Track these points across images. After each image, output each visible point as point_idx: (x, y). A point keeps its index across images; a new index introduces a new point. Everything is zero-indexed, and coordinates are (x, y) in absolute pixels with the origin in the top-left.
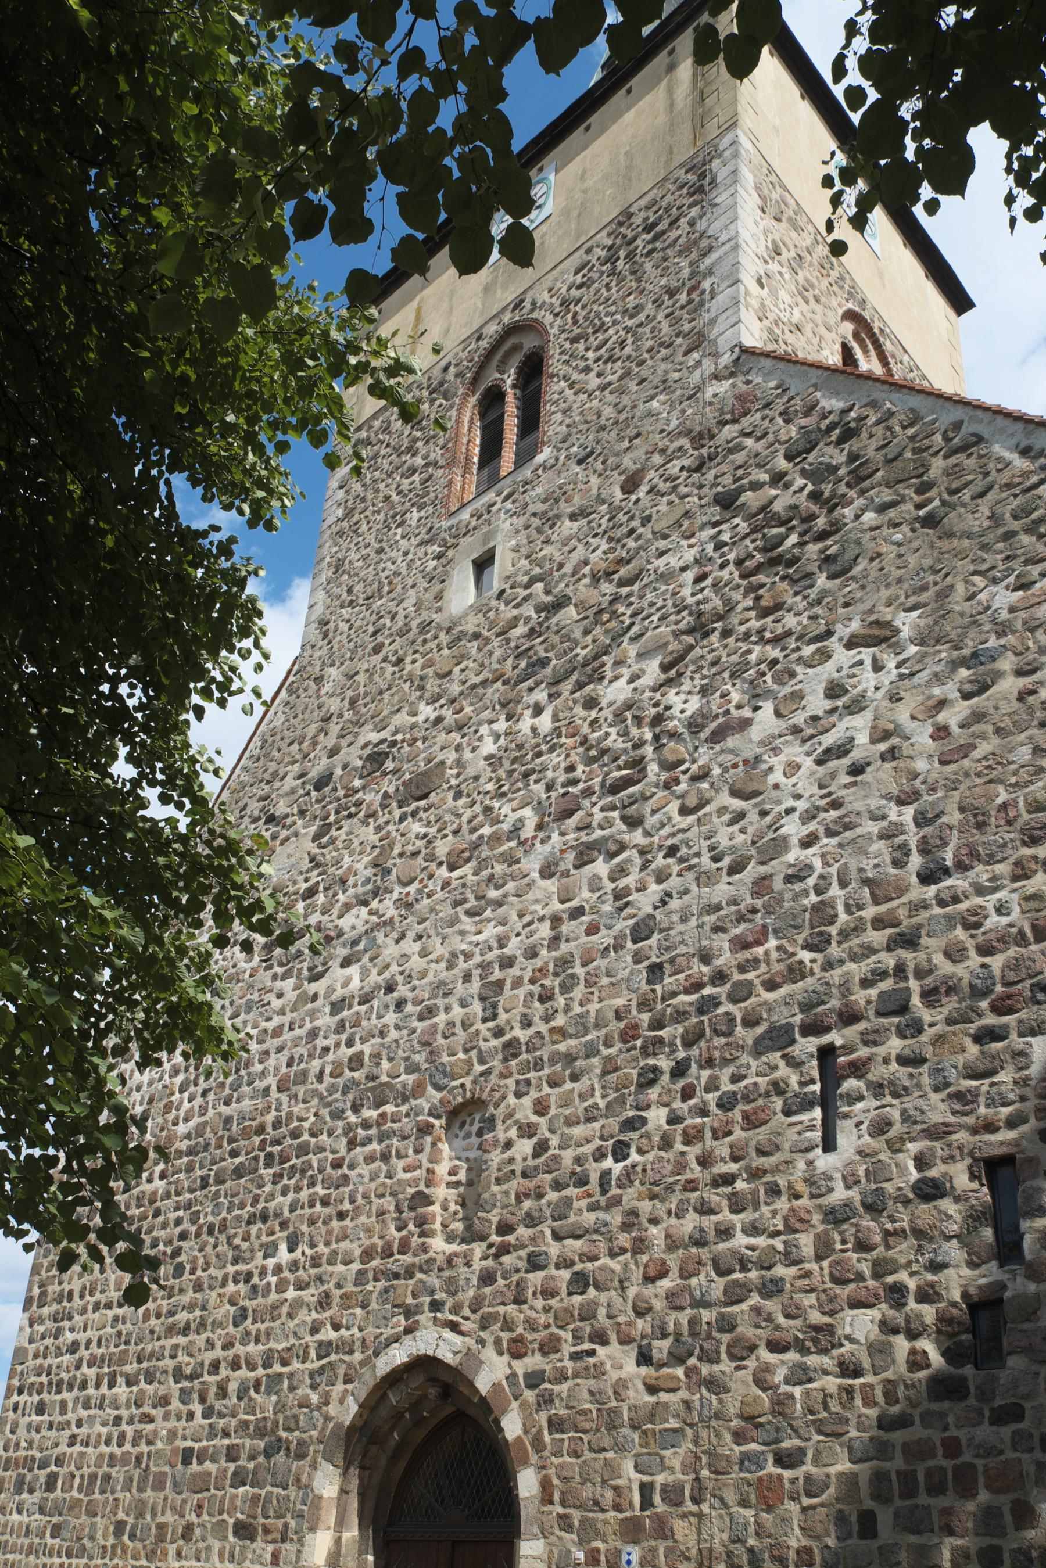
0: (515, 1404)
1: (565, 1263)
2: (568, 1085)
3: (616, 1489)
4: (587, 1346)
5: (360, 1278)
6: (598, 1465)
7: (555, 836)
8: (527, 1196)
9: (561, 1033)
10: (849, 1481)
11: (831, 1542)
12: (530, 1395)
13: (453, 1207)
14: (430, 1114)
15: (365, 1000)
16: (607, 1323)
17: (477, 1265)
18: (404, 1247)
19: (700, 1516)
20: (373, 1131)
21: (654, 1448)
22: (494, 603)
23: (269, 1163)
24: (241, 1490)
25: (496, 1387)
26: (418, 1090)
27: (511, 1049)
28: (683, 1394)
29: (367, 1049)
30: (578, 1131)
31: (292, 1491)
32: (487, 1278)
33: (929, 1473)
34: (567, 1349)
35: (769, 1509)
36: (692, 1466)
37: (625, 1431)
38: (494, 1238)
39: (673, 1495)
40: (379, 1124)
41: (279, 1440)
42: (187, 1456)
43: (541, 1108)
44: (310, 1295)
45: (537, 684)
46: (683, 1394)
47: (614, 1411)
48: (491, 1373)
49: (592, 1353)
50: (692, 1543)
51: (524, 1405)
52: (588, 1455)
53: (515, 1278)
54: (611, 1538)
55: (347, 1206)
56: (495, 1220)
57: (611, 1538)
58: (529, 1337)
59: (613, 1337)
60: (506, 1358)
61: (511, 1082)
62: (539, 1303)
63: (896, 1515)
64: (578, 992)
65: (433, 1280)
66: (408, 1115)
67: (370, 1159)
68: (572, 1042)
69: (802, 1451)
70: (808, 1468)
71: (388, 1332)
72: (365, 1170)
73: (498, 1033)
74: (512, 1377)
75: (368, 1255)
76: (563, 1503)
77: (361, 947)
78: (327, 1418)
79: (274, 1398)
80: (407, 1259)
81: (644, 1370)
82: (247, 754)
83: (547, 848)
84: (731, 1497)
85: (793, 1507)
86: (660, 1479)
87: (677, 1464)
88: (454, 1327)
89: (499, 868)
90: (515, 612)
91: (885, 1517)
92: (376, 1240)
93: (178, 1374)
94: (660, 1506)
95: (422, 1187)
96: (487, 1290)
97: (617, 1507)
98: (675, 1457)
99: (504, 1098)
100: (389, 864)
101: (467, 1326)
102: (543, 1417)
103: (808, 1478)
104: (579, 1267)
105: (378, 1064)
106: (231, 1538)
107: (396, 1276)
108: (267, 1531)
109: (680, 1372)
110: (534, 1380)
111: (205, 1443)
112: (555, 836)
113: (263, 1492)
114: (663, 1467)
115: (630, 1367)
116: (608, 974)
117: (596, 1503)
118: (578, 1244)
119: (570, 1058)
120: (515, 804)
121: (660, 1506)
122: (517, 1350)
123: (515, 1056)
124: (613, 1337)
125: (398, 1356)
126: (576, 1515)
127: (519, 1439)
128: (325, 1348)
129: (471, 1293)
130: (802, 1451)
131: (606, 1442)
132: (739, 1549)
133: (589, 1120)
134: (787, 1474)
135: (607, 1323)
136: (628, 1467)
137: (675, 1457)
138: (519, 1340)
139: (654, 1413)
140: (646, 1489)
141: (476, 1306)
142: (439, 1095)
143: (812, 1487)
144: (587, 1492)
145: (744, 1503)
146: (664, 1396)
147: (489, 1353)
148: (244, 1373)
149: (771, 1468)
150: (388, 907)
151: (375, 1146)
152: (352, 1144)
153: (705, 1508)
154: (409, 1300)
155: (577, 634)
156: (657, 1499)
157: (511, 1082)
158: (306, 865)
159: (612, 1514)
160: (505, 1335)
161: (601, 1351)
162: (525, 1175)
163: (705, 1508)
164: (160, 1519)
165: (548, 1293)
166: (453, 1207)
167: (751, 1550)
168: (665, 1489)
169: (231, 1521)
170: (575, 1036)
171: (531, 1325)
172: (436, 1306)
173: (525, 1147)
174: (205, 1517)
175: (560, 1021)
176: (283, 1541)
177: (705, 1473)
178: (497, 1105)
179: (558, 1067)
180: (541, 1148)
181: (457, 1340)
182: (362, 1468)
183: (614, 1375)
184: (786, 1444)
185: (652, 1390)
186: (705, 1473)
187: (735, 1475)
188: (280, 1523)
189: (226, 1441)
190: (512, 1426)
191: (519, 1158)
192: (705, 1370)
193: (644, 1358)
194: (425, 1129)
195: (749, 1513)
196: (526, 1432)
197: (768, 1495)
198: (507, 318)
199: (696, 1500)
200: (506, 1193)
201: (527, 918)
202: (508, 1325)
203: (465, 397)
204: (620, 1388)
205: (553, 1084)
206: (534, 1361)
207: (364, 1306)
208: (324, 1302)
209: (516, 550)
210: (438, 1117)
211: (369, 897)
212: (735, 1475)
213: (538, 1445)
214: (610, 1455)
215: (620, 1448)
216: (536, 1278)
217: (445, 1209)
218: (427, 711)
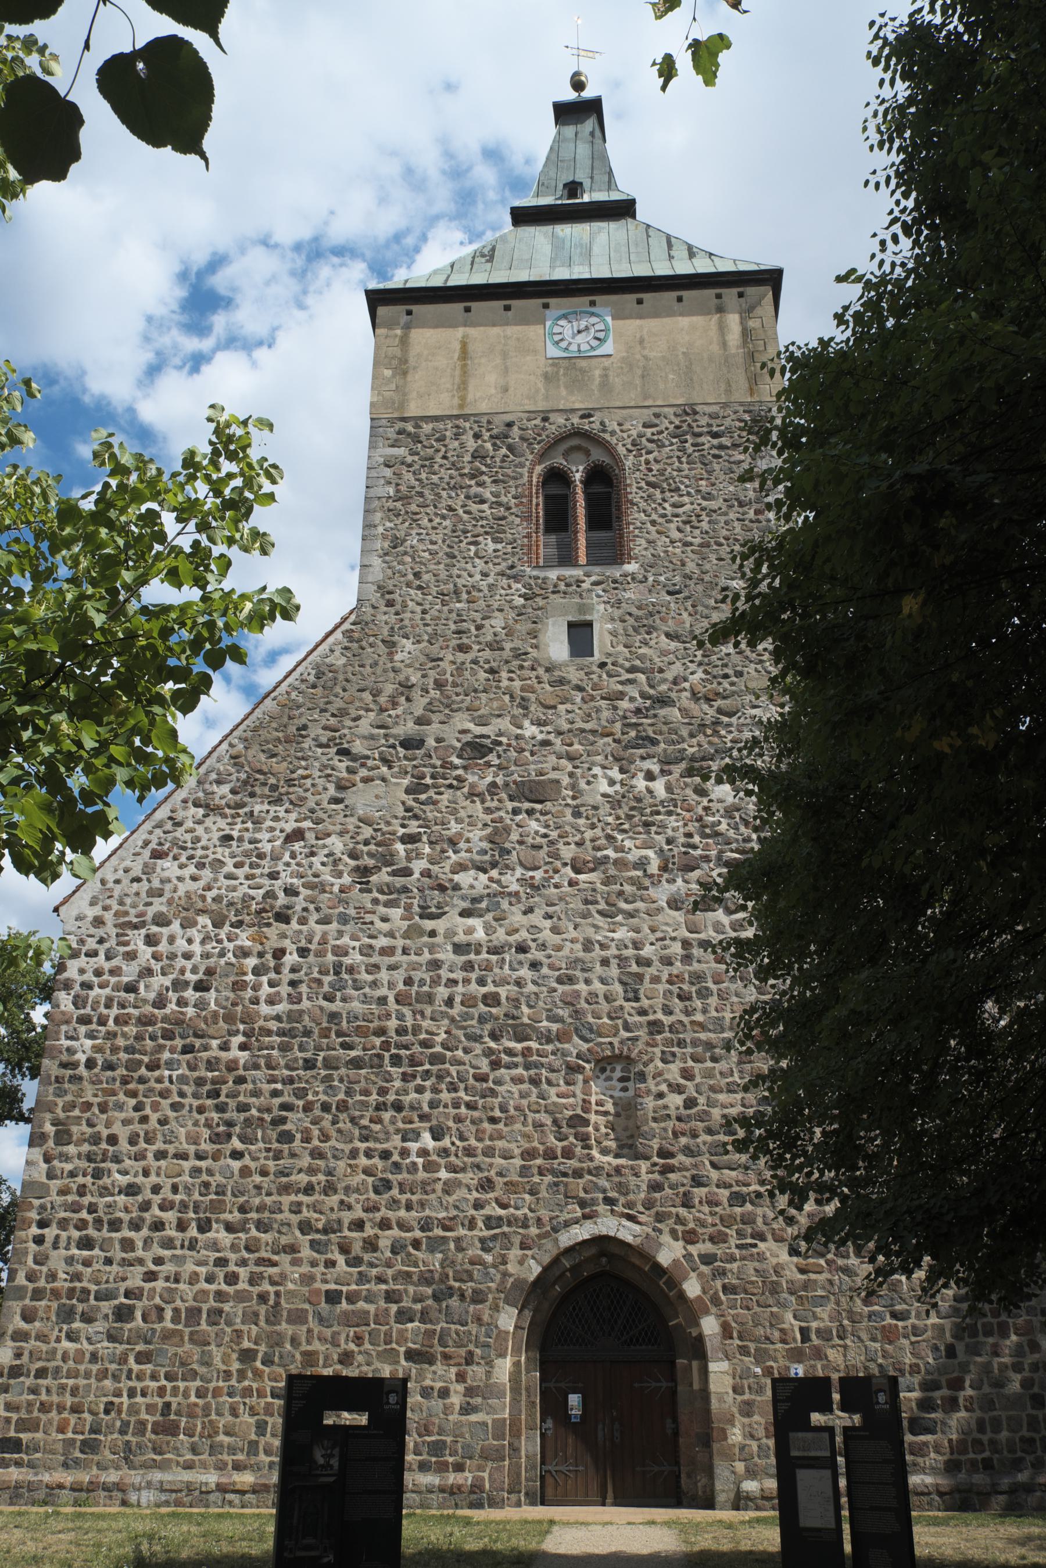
0: (693, 1274)
1: (722, 1184)
2: (709, 1064)
3: (782, 1330)
4: (749, 1241)
5: (524, 1171)
6: (767, 1315)
7: (679, 881)
8: (683, 1134)
9: (702, 1026)
10: (940, 1329)
11: (931, 1360)
12: (704, 1269)
13: (603, 1130)
14: (578, 1056)
15: (494, 951)
16: (765, 1228)
17: (645, 1177)
18: (568, 1153)
19: (845, 1347)
20: (519, 1059)
21: (807, 1306)
22: (595, 668)
23: (396, 1060)
24: (410, 1325)
25: (676, 1262)
26: (562, 1037)
27: (655, 1027)
28: (825, 1275)
29: (503, 992)
30: (722, 1097)
31: (473, 1328)
32: (655, 1187)
33: (984, 1325)
34: (733, 1241)
35: (890, 1343)
36: (836, 1316)
37: (785, 1295)
38: (656, 1159)
39: (824, 1334)
40: (524, 1055)
41: (451, 1288)
42: (333, 1298)
43: (687, 1074)
44: (469, 1178)
45: (650, 756)
46: (825, 1275)
47: (777, 1283)
48: (669, 1253)
49: (755, 1246)
50: (840, 1360)
51: (701, 1276)
52: (757, 1309)
53: (682, 1190)
54: (781, 1360)
55: (497, 1113)
56: (656, 1147)
57: (781, 1360)
58: (700, 1230)
59: (769, 1237)
60: (681, 1243)
61: (657, 1051)
62: (706, 1209)
63: (967, 1346)
64: (713, 1001)
65: (603, 1182)
66: (553, 1053)
67: (517, 1080)
68: (712, 1035)
69: (908, 1312)
70: (913, 1320)
71: (565, 1216)
72: (509, 1086)
73: (642, 1012)
74: (688, 1256)
75: (529, 1154)
76: (741, 1338)
77: (483, 905)
78: (505, 1274)
79: (439, 1256)
80: (573, 1163)
81: (795, 1259)
82: (296, 675)
83: (673, 888)
84: (864, 1336)
85: (905, 1342)
86: (814, 1325)
87: (825, 1316)
88: (631, 1218)
89: (628, 888)
90: (620, 687)
91: (960, 1348)
92: (536, 1144)
93: (305, 1227)
94: (815, 1341)
95: (579, 1111)
96: (657, 1195)
97: (784, 1341)
98: (824, 1313)
99: (652, 1060)
100: (507, 845)
101: (642, 1218)
102: (718, 1284)
103: (914, 1327)
104: (736, 1189)
105: (517, 1008)
106: (403, 1362)
107: (565, 1175)
108: (446, 1357)
109: (822, 1262)
110: (707, 1259)
111: (354, 1287)
112: (679, 881)
113: (438, 1328)
114: (815, 1317)
115: (784, 1257)
116: (737, 995)
117: (767, 1338)
118: (734, 1173)
119: (709, 1046)
120: (638, 843)
121: (815, 1341)
122: (690, 1238)
123: (659, 1033)
124: (769, 1237)
125: (582, 1232)
126: (752, 1346)
127: (699, 1298)
128: (490, 1222)
129: (642, 1195)
130: (908, 1312)
131: (771, 1301)
132: (872, 1365)
133: (730, 1091)
134: (900, 1324)
135: (765, 1228)
136: (789, 1316)
137: (824, 1313)
138: (693, 1232)
139: (806, 1286)
140: (805, 1332)
141: (648, 1205)
142: (586, 1046)
143: (916, 1331)
144: (760, 1331)
145: (874, 1339)
146: (813, 1276)
147: (666, 1238)
148: (395, 1232)
149: (889, 1320)
150: (512, 881)
151: (520, 1071)
152: (495, 1065)
153: (848, 1342)
154: (582, 1194)
155: (685, 733)
156: (813, 1337)
157: (657, 1051)
158: (400, 811)
159: (779, 1346)
160: (679, 1228)
161: (762, 1245)
162: (679, 1119)
163: (848, 1342)
164: (305, 1347)
165: (712, 1203)
166: (603, 1130)
167: (880, 1366)
168: (818, 1331)
169: (402, 1349)
170: (714, 1031)
171: (702, 1224)
172: (609, 1201)
173: (676, 1100)
174: (367, 1346)
175: (699, 1017)
176: (468, 1364)
177: (846, 1322)
178: (646, 1065)
179: (700, 1049)
180: (691, 1103)
181: (637, 1228)
182: (536, 1311)
183: (774, 1261)
184: (898, 1307)
185: (802, 1271)
186: (846, 1322)
187: (865, 1323)
188: (462, 1352)
189: (384, 1287)
190: (692, 1288)
191: (672, 1107)
192: (840, 1262)
193: (794, 1252)
194: (576, 1069)
195: (878, 1345)
196: (704, 1292)
197: (889, 1335)
198: (576, 420)
199: (840, 1338)
200: (665, 1129)
201: (659, 935)
202: (680, 1221)
203: (534, 464)
204: (778, 1270)
205: (696, 1059)
206: (707, 1247)
207: (532, 1193)
208: (487, 1185)
209: (614, 634)
210: (588, 1062)
211: (488, 866)
212: (865, 1323)
213: (716, 1301)
214: (775, 1309)
215: (783, 1306)
216: (700, 1192)
217: (597, 1130)
218: (530, 730)
